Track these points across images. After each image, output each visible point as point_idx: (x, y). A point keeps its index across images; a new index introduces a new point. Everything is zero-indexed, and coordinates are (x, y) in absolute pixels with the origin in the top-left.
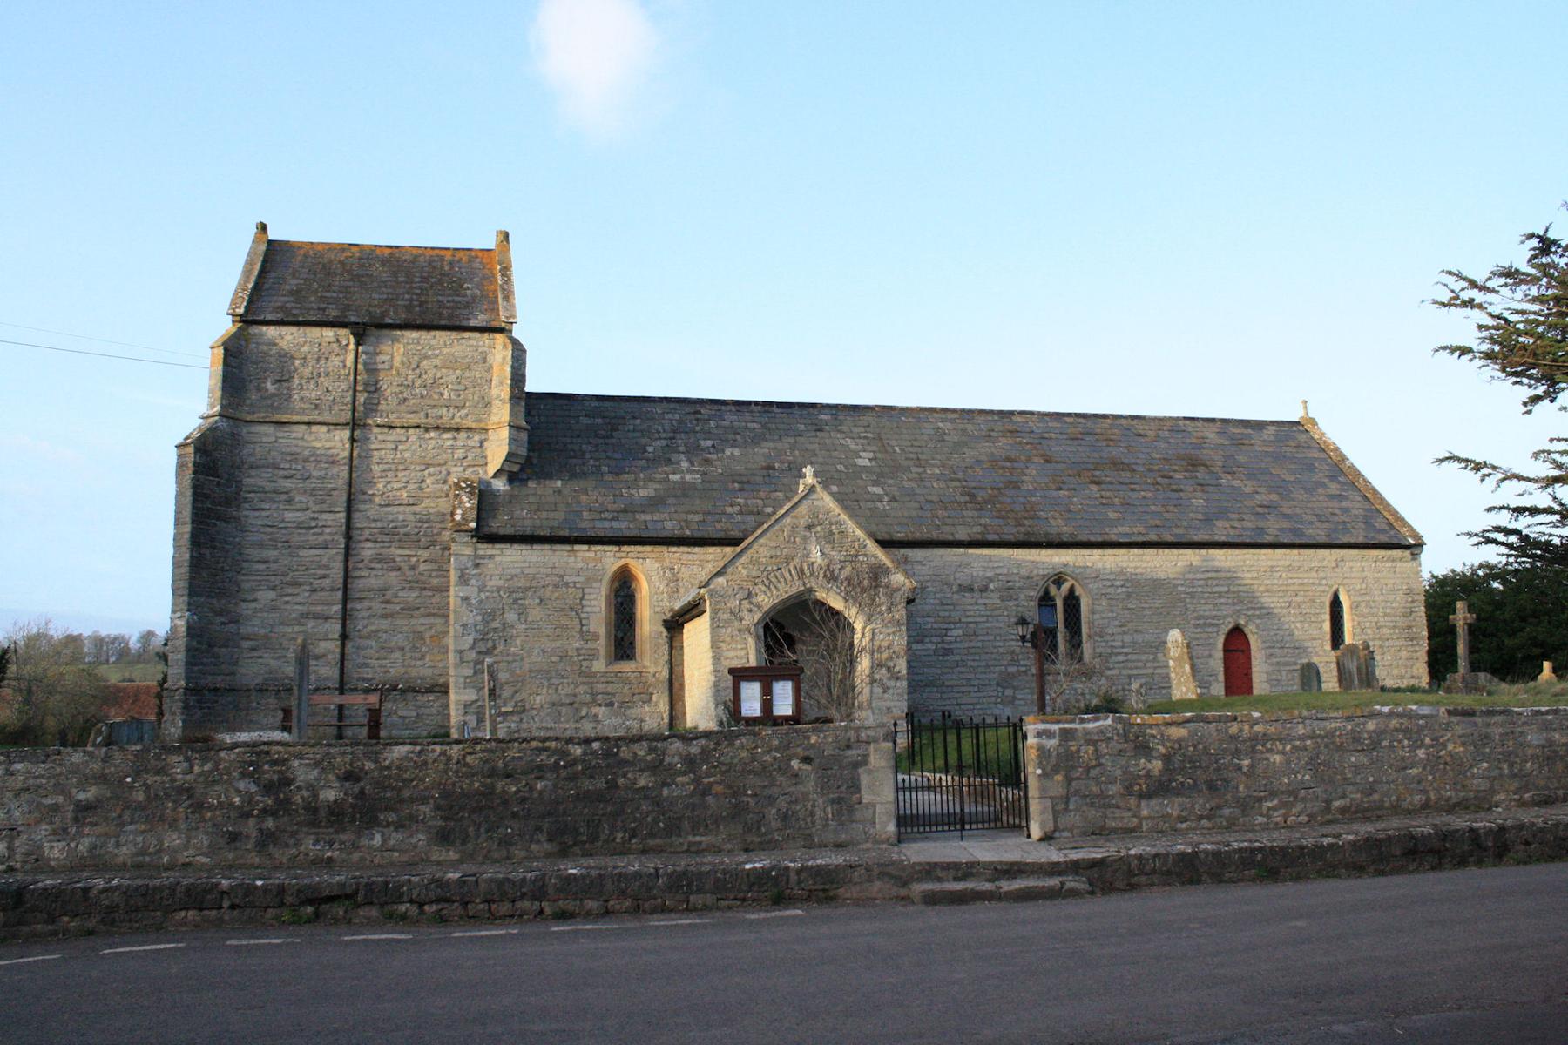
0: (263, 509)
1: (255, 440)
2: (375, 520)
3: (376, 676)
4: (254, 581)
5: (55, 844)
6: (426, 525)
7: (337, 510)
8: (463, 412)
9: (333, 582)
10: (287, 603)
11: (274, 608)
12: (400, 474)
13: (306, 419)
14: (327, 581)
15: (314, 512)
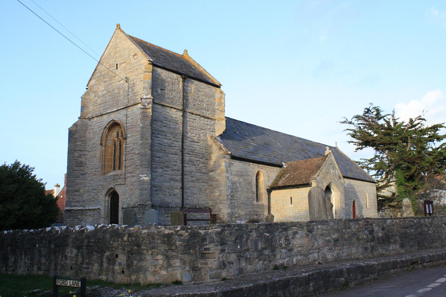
0: (159, 137)
1: (156, 110)
2: (189, 147)
3: (190, 203)
4: (156, 164)
5: (329, 254)
6: (201, 150)
7: (179, 141)
8: (209, 112)
9: (178, 167)
10: (165, 174)
11: (162, 176)
12: (195, 131)
13: (170, 106)
14: (177, 167)
15: (173, 141)
